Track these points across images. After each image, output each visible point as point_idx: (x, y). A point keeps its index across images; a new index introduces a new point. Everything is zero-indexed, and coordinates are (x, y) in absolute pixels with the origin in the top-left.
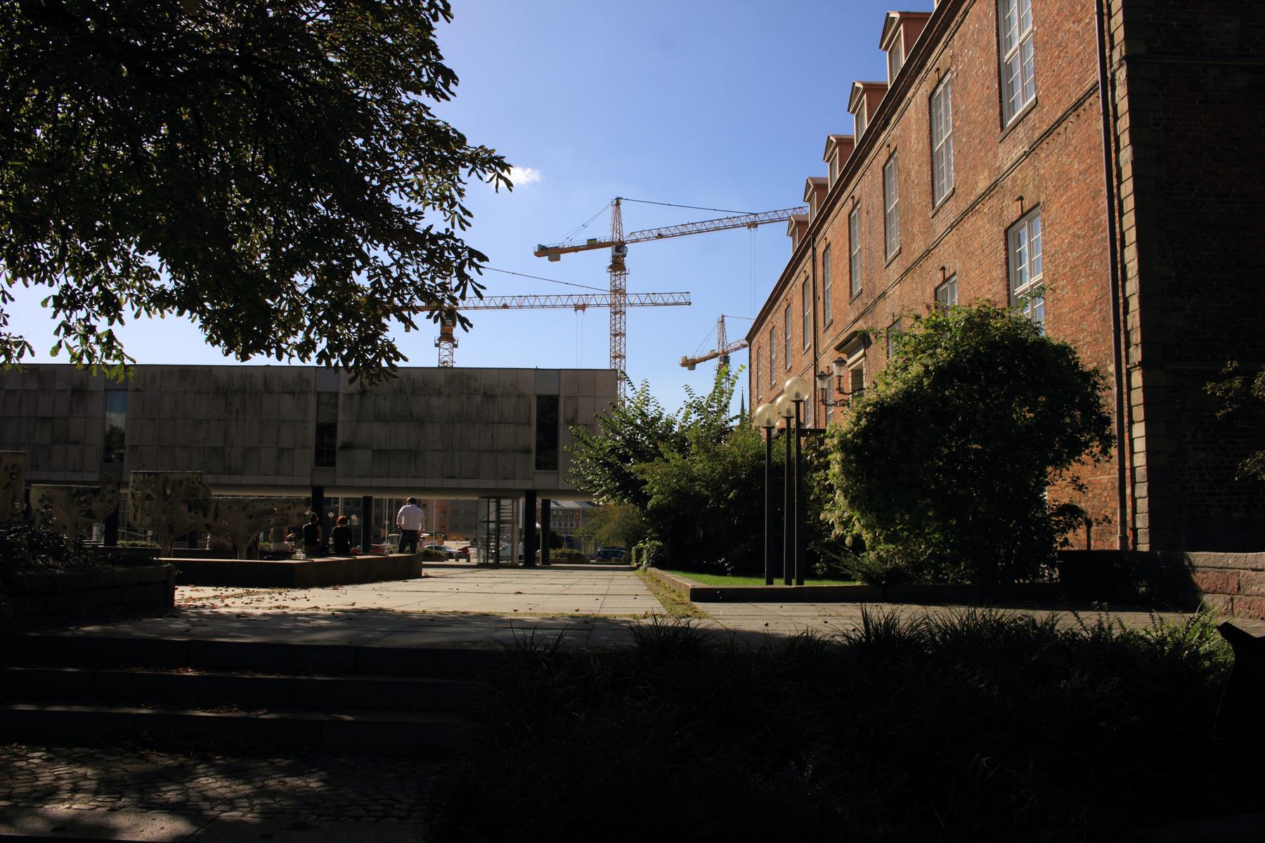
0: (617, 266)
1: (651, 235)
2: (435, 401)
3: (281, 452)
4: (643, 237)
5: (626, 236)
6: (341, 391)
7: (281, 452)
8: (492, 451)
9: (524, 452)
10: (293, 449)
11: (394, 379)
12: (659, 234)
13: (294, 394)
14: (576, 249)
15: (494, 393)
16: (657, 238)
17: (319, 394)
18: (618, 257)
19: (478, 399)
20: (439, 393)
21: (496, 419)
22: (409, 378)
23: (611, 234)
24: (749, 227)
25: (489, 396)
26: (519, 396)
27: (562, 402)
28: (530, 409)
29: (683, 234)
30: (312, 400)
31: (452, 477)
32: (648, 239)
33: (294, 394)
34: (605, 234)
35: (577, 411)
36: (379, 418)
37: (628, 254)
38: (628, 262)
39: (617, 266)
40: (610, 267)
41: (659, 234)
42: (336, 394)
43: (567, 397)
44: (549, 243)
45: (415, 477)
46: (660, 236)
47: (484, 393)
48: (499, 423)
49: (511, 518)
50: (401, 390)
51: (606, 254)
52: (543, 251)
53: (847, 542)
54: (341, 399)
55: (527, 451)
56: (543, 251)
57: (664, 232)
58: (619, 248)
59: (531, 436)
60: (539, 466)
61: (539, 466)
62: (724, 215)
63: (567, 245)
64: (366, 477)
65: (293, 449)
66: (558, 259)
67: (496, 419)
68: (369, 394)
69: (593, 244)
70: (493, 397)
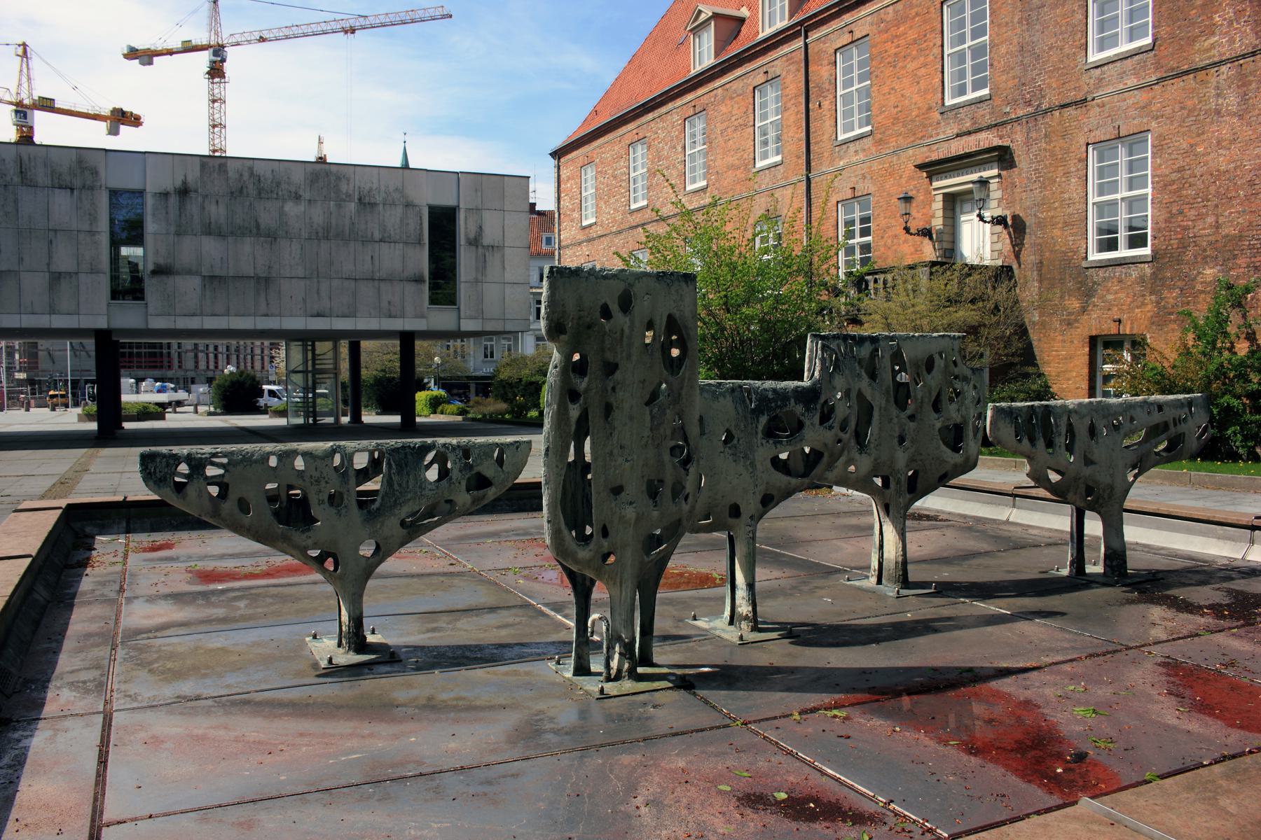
0: (216, 72)
1: (253, 38)
2: (291, 208)
3: (56, 278)
4: (243, 39)
5: (225, 38)
6: (148, 190)
7: (56, 278)
8: (373, 280)
9: (416, 281)
10: (77, 273)
11: (955, 131)
12: (261, 37)
13: (72, 190)
14: (170, 53)
15: (373, 201)
16: (259, 41)
17: (114, 193)
18: (215, 62)
19: (352, 206)
20: (297, 197)
21: (377, 236)
22: (252, 174)
23: (207, 35)
24: (346, 32)
25: (366, 203)
26: (406, 206)
27: (461, 216)
28: (421, 224)
29: (287, 37)
30: (104, 200)
31: (318, 315)
32: (249, 42)
33: (72, 190)
34: (201, 37)
35: (481, 227)
36: (210, 230)
37: (228, 60)
38: (227, 67)
39: (216, 72)
40: (208, 73)
41: (261, 37)
42: (141, 193)
43: (468, 210)
44: (141, 45)
45: (266, 315)
46: (262, 40)
47: (360, 199)
48: (381, 241)
49: (331, 366)
50: (241, 191)
51: (203, 60)
52: (132, 54)
53: (1165, 444)
54: (150, 201)
55: (418, 280)
56: (132, 54)
57: (266, 35)
58: (218, 51)
59: (421, 260)
60: (433, 301)
61: (433, 301)
62: (329, 17)
63: (159, 46)
64: (194, 315)
65: (77, 273)
66: (151, 63)
67: (377, 236)
68: (193, 195)
69: (189, 48)
70: (373, 205)
